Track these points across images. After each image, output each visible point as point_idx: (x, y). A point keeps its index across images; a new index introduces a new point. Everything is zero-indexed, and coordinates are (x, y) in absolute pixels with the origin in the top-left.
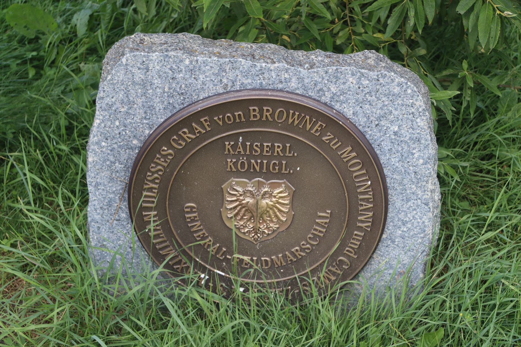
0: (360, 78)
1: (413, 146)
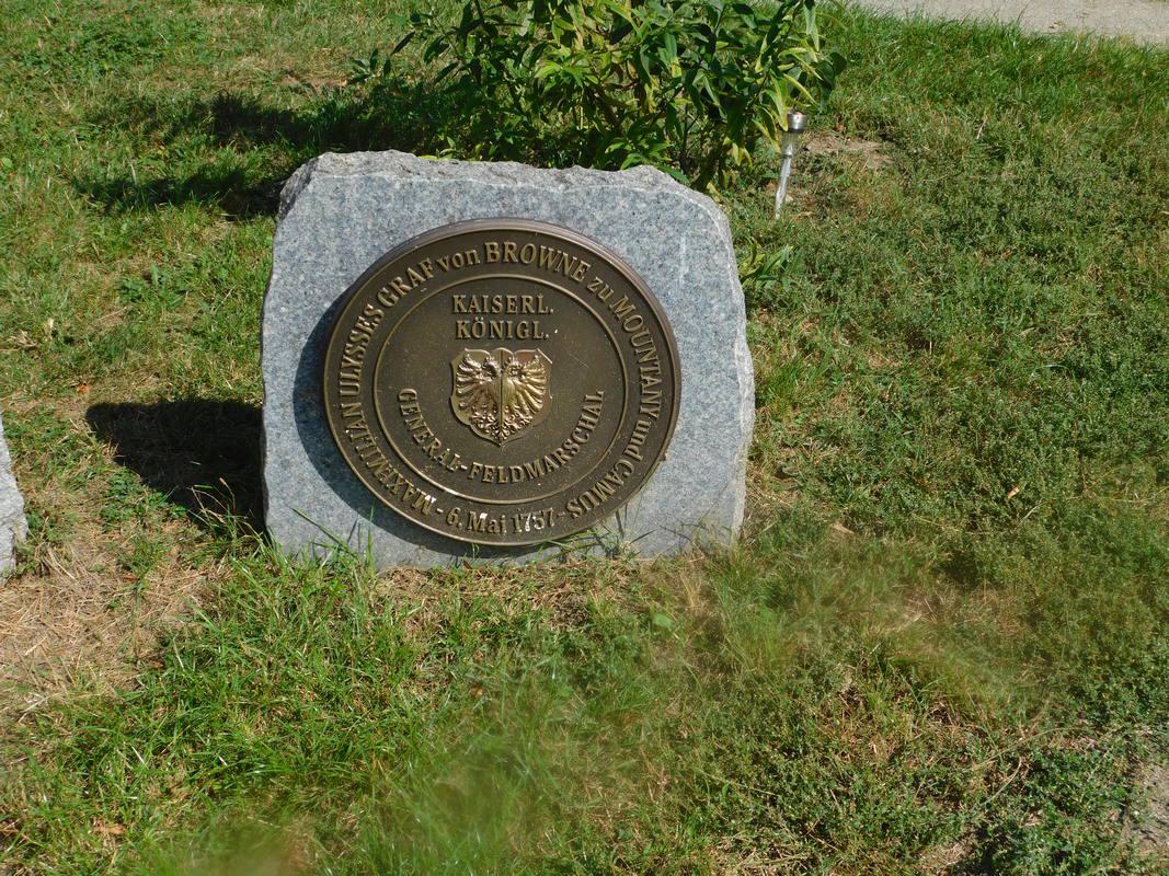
0: (634, 201)
1: (712, 294)
